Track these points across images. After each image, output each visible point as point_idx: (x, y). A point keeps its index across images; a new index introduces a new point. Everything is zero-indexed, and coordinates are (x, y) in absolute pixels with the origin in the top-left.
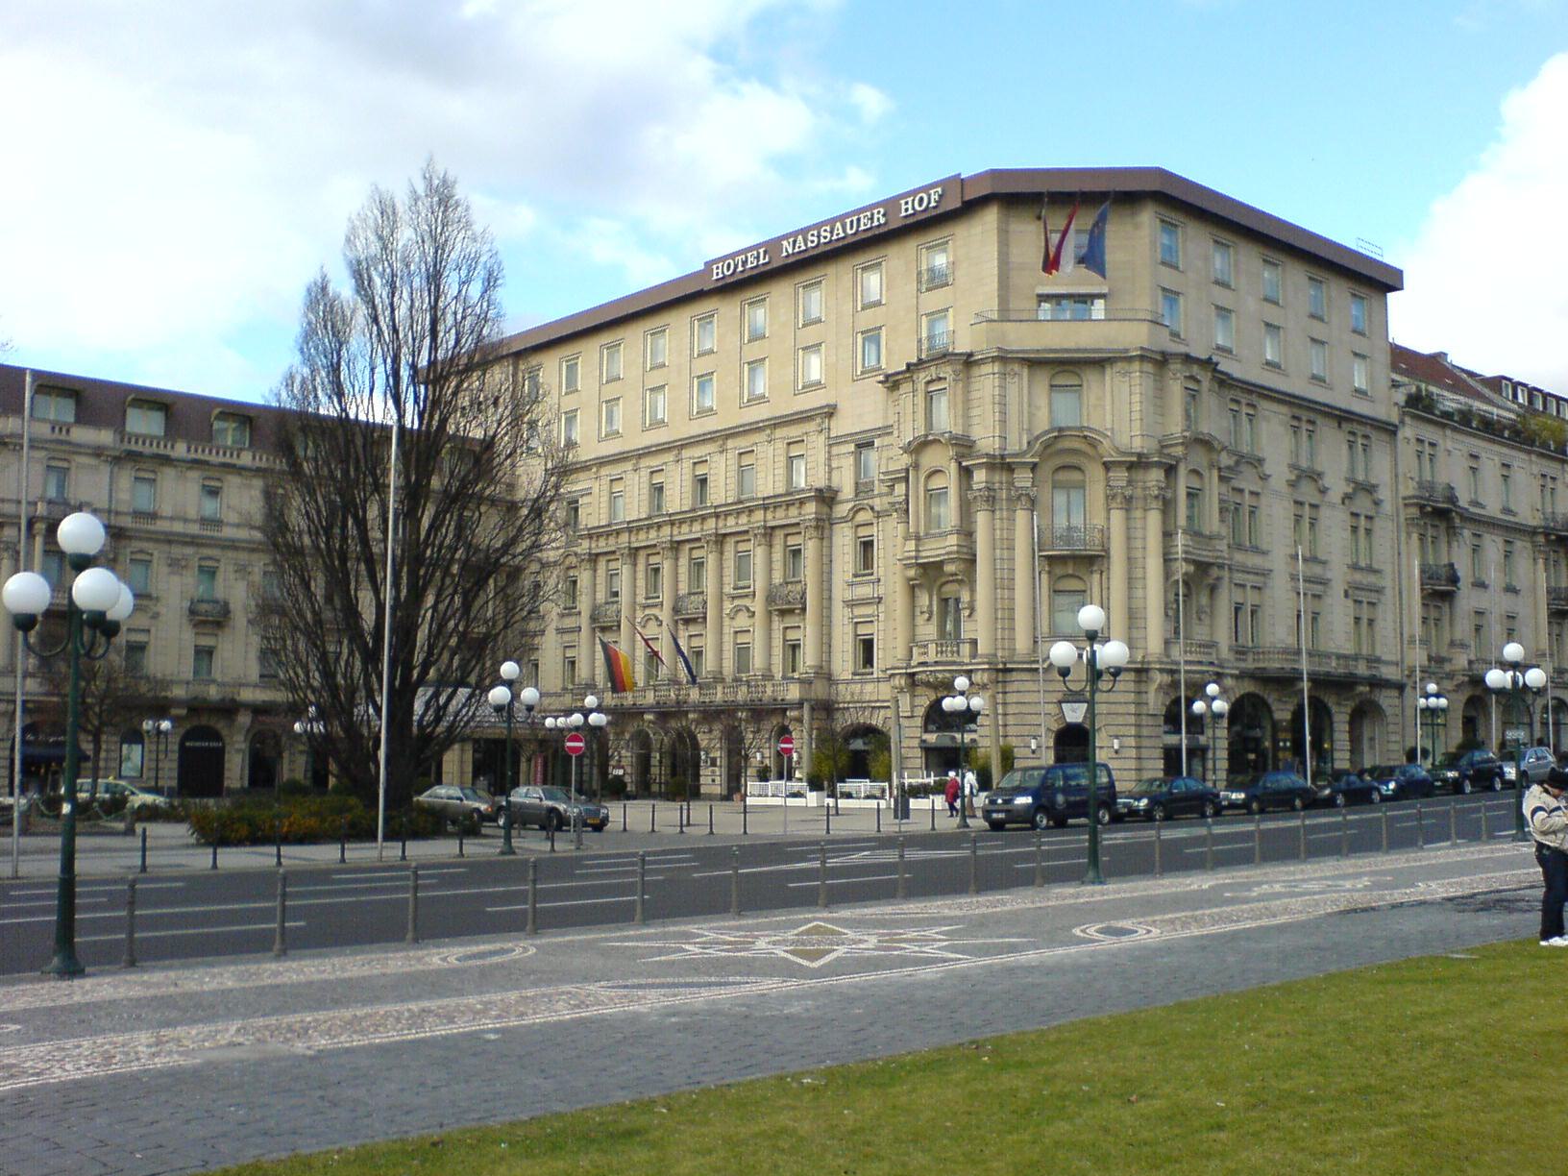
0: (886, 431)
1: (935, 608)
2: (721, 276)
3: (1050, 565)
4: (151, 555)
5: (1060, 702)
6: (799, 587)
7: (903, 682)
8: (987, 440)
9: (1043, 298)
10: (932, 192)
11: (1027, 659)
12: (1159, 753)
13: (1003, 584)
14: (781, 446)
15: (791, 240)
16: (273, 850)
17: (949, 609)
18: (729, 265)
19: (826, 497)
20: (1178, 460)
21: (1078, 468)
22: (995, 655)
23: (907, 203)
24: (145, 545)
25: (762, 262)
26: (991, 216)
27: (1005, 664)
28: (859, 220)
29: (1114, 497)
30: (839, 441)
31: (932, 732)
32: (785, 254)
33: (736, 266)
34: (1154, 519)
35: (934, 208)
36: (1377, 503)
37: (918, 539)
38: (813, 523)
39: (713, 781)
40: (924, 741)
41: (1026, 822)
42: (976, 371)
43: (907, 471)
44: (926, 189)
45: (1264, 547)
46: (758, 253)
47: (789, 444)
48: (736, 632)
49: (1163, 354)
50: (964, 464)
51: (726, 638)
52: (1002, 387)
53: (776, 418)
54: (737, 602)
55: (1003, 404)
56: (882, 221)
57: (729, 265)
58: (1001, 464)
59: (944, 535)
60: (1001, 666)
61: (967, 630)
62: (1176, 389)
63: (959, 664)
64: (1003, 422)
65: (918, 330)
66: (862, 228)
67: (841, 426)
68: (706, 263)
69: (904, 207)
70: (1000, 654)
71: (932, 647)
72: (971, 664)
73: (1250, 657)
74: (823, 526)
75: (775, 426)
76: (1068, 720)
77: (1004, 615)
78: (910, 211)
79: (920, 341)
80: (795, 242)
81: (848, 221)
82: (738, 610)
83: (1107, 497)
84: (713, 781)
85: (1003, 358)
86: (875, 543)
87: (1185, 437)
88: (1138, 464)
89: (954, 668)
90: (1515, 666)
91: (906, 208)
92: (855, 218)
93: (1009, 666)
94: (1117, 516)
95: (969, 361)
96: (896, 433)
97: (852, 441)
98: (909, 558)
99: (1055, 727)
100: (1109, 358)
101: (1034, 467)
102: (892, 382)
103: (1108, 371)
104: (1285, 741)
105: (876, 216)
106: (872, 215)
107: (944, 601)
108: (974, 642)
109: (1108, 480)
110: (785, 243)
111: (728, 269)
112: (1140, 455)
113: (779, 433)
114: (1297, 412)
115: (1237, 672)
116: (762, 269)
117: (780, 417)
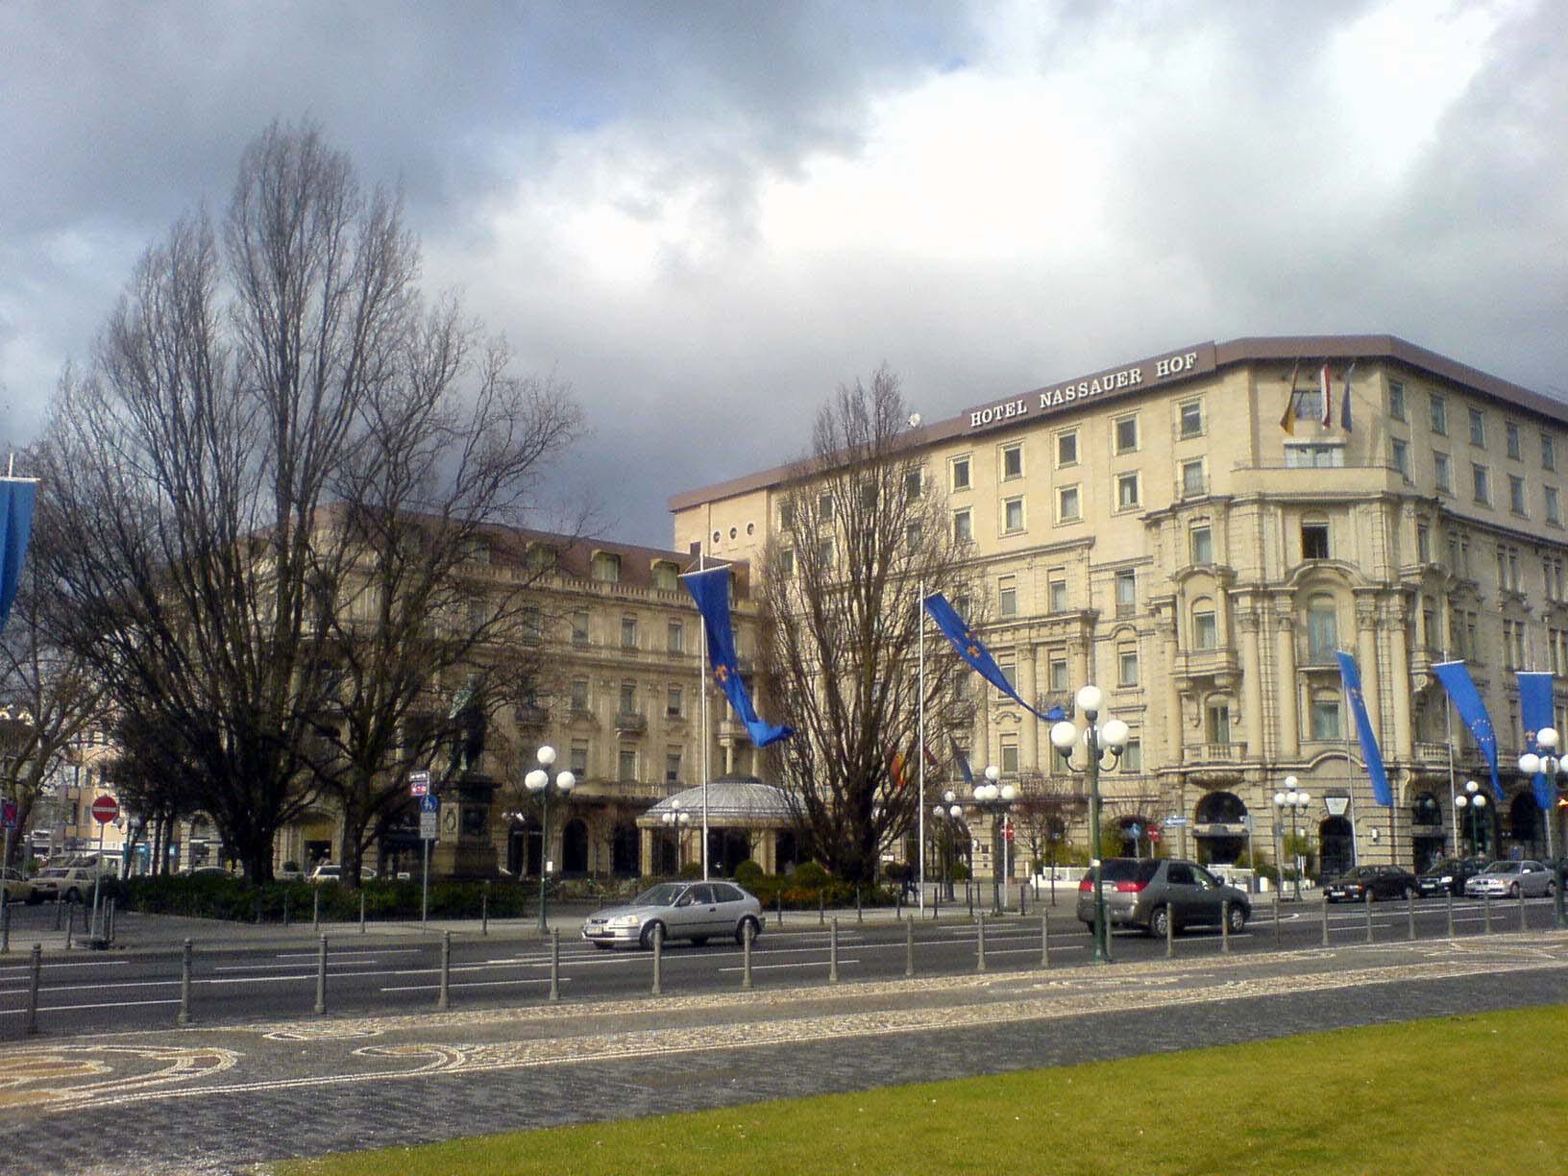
0: (1146, 560)
1: (1203, 717)
2: (979, 423)
3: (1309, 678)
4: (588, 677)
5: (1325, 797)
6: (1066, 697)
7: (1176, 780)
8: (1247, 571)
9: (1289, 446)
10: (1187, 356)
11: (1292, 760)
12: (1409, 841)
13: (1267, 695)
14: (1041, 574)
15: (1049, 394)
16: (818, 913)
17: (1218, 717)
18: (987, 414)
19: (1089, 618)
20: (1416, 587)
21: (1330, 596)
22: (1264, 756)
23: (1163, 365)
24: (584, 670)
25: (1020, 412)
26: (1241, 380)
27: (1274, 764)
28: (1116, 378)
29: (1363, 621)
30: (1098, 569)
31: (1204, 823)
32: (1043, 406)
33: (994, 415)
34: (1398, 638)
35: (1191, 370)
36: (1479, 600)
37: (1187, 656)
38: (1079, 641)
39: (985, 866)
40: (1197, 831)
41: (201, 954)
42: (1235, 512)
43: (1175, 597)
44: (1182, 353)
45: (1481, 659)
46: (1017, 405)
47: (1049, 571)
48: (1002, 735)
49: (1399, 496)
50: (1230, 592)
51: (991, 740)
52: (1261, 525)
53: (1036, 548)
54: (1003, 709)
55: (1262, 540)
56: (1139, 380)
57: (987, 414)
58: (1262, 592)
59: (1214, 652)
60: (1270, 766)
61: (1235, 735)
62: (1409, 525)
63: (1232, 764)
64: (1262, 555)
65: (1174, 475)
66: (1119, 385)
67: (1098, 556)
68: (963, 412)
69: (1159, 369)
70: (1267, 754)
71: (1205, 750)
72: (1242, 764)
73: (1476, 757)
74: (1087, 643)
75: (1035, 555)
76: (1332, 813)
77: (1269, 722)
78: (1166, 372)
79: (1176, 483)
80: (1052, 396)
81: (1105, 379)
82: (1005, 715)
83: (1357, 619)
84: (985, 866)
85: (1262, 501)
86: (1138, 658)
87: (1422, 568)
88: (1383, 592)
89: (1227, 767)
90: (1548, 751)
91: (1163, 370)
92: (1112, 377)
93: (1277, 766)
94: (1366, 637)
95: (1229, 503)
96: (1156, 564)
97: (1112, 569)
98: (1180, 673)
99: (1320, 819)
100: (1352, 501)
101: (1292, 595)
102: (1153, 521)
103: (1351, 511)
104: (1506, 832)
105: (1133, 376)
106: (1129, 374)
107: (1213, 712)
108: (1244, 746)
109: (1357, 605)
110: (1043, 396)
111: (986, 418)
112: (1385, 584)
113: (1038, 561)
114: (1503, 541)
115: (1469, 771)
116: (1020, 418)
117: (1041, 547)
